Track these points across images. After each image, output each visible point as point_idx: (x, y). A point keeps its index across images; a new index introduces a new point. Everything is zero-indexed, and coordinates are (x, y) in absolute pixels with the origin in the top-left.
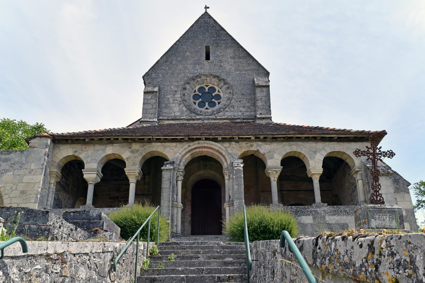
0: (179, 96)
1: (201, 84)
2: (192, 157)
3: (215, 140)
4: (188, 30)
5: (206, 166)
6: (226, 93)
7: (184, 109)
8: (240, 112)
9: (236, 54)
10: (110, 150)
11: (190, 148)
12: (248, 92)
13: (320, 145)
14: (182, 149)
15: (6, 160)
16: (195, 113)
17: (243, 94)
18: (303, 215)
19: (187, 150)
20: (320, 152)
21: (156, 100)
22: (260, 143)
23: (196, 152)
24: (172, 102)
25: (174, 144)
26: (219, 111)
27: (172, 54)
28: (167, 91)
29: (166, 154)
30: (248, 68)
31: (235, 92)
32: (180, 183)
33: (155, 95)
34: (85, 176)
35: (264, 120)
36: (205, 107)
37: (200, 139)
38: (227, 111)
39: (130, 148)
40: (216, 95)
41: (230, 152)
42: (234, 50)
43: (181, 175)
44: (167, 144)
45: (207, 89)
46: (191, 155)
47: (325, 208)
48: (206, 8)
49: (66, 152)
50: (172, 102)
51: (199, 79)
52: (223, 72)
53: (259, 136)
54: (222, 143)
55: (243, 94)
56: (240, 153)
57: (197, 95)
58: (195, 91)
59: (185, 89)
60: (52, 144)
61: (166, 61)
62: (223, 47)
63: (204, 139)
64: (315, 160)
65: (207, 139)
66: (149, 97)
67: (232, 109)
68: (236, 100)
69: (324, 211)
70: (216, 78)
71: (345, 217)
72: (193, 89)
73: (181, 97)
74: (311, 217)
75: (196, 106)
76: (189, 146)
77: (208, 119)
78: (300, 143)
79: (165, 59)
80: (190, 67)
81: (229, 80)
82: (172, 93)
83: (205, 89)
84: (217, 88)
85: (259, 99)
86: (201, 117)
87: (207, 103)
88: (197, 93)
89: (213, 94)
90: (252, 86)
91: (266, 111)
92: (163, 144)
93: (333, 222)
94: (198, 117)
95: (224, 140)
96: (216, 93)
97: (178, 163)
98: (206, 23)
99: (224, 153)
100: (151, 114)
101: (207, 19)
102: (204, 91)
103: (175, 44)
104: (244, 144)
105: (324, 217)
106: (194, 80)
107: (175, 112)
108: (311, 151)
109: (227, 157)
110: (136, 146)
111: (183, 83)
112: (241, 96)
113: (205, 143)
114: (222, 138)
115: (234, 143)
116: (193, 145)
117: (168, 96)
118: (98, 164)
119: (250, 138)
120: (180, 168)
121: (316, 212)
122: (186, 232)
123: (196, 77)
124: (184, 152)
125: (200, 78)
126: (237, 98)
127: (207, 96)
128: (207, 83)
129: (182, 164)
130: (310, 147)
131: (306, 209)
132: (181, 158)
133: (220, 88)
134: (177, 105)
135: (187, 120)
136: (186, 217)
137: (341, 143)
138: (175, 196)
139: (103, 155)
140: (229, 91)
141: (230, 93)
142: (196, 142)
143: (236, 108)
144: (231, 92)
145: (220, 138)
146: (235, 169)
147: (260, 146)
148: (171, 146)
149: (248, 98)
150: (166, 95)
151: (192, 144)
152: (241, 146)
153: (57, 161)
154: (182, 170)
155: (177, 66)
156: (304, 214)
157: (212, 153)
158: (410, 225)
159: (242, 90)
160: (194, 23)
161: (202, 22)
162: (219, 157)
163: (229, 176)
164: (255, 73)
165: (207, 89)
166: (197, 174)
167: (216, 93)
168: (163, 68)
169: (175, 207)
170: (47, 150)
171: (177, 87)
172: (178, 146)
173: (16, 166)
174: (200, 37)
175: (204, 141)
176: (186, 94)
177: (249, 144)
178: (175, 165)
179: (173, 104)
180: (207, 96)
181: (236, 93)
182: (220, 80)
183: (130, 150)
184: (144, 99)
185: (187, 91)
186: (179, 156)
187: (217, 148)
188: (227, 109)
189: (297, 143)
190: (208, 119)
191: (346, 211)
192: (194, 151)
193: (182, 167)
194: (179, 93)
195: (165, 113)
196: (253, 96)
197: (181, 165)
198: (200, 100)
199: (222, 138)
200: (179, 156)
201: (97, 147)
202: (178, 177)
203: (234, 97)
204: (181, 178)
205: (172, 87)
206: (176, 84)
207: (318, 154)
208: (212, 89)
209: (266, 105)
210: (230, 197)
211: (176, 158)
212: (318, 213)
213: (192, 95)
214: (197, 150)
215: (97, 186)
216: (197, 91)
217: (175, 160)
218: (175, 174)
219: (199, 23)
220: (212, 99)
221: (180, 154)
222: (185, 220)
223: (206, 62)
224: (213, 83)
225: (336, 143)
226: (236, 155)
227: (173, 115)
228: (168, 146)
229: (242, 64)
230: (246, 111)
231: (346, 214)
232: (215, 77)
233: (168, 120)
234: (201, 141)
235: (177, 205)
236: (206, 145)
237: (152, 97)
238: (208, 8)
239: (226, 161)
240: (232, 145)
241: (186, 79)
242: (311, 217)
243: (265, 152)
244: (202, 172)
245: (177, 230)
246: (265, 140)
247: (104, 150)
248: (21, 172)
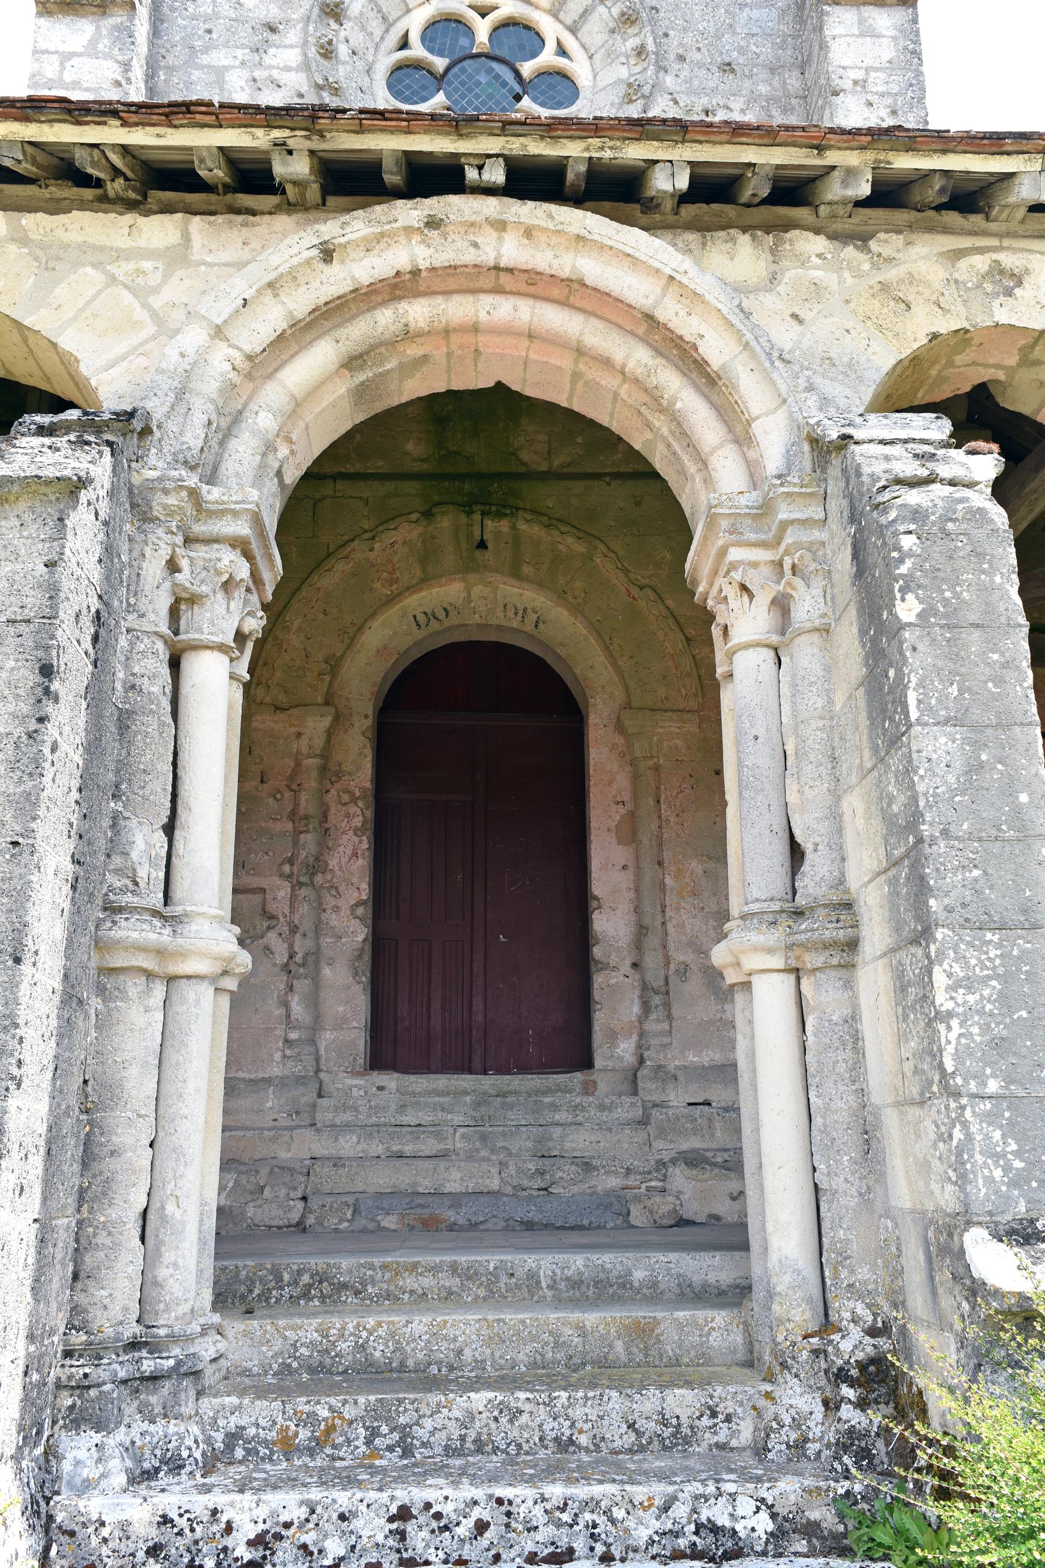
0: (292, 57)
2: (360, 393)
5: (482, 545)
6: (611, 56)
12: (766, 50)
14: (242, 286)
17: (728, 67)
19: (301, 301)
21: (127, 66)
23: (408, 335)
25: (158, 230)
28: (207, 18)
29: (67, 342)
31: (673, 45)
32: (215, 688)
33: (118, 28)
40: (543, 74)
41: (785, 335)
43: (228, 586)
44: (85, 227)
45: (482, 29)
46: (352, 362)
54: (692, 237)
55: (728, 67)
56: (883, 358)
57: (416, 65)
58: (404, 44)
63: (496, 175)
65: (533, 181)
72: (388, 24)
73: (306, 66)
76: (327, 254)
82: (244, 34)
83: (469, 31)
84: (550, 29)
85: (847, 84)
88: (417, 51)
89: (527, 69)
90: (783, 12)
92: (29, 221)
96: (548, 57)
97: (194, 437)
99: (716, 349)
102: (464, 42)
109: (752, 391)
112: (715, 79)
113: (500, 226)
115: (812, 244)
116: (369, 245)
117: (219, 58)
120: (212, 494)
122: (328, 1035)
124: (269, 320)
126: (690, 92)
127: (483, 78)
129: (242, 455)
132: (230, 389)
133: (573, 30)
136: (332, 918)
138: (144, 842)
140: (633, 42)
141: (640, 52)
142: (409, 212)
144: (651, 47)
145: (668, 182)
146: (917, 514)
148: (121, 255)
149: (763, 89)
150: (206, 50)
151: (356, 225)
152: (891, 274)
154: (242, 528)
157: (580, 351)
159: (718, 37)
162: (654, 398)
163: (782, 605)
165: (482, 29)
166: (417, 602)
167: (548, 57)
169: (134, 986)
172: (197, 252)
175: (492, 205)
176: (343, 50)
177: (981, 262)
178: (154, 466)
180: (483, 78)
181: (681, 58)
186: (202, 359)
187: (636, 289)
192: (385, 319)
193: (250, 489)
194: (293, 36)
196: (794, 82)
197: (229, 467)
200: (202, 359)
202: (194, 600)
203: (669, 81)
204: (228, 617)
210: (796, 853)
211: (166, 384)
214: (418, 312)
216: (414, 38)
217: (157, 408)
218: (153, 568)
220: (518, 98)
221: (219, 332)
222: (326, 941)
226: (851, 369)
228: (84, 247)
235: (161, 953)
236: (511, 251)
237: (93, 42)
239: (740, 432)
240: (803, 262)
244: (450, 591)
245: (148, 1288)
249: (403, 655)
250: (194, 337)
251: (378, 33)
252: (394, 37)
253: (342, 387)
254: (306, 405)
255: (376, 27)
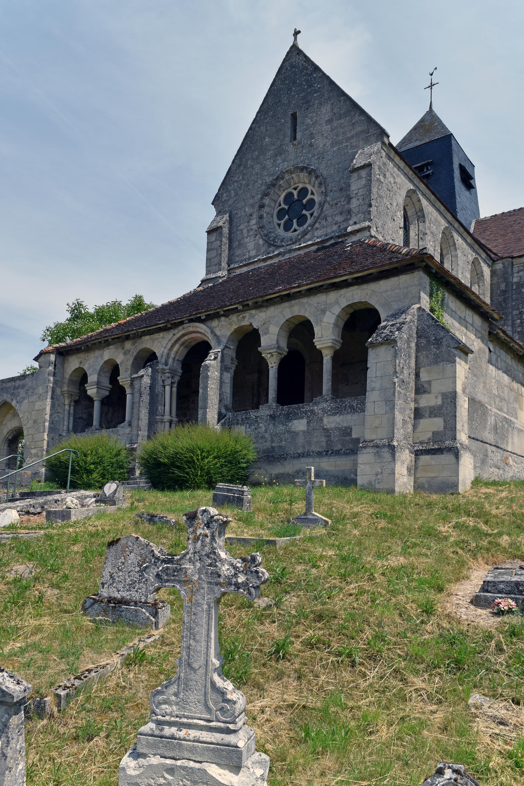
1: (287, 189)
3: (199, 320)
4: (267, 95)
7: (261, 242)
8: (336, 224)
9: (335, 111)
10: (107, 354)
11: (175, 338)
13: (333, 296)
15: (23, 386)
16: (274, 246)
18: (296, 419)
19: (173, 341)
20: (331, 310)
22: (253, 312)
24: (246, 235)
25: (161, 334)
26: (305, 233)
27: (247, 150)
28: (240, 217)
30: (353, 132)
31: (329, 188)
34: (89, 392)
35: (358, 235)
36: (309, 216)
37: (182, 323)
38: (317, 229)
39: (123, 349)
41: (218, 333)
42: (332, 104)
44: (156, 336)
47: (324, 405)
48: (297, 33)
49: (73, 363)
50: (246, 235)
51: (281, 182)
52: (314, 156)
53: (246, 303)
59: (262, 206)
60: (60, 359)
61: (240, 166)
62: (315, 106)
64: (323, 324)
65: (191, 321)
66: (213, 239)
67: (324, 223)
68: (331, 203)
69: (323, 409)
70: (305, 171)
71: (349, 417)
72: (275, 202)
74: (304, 421)
75: (281, 231)
76: (174, 335)
77: (290, 251)
78: (305, 300)
79: (237, 161)
80: (269, 163)
81: (323, 170)
85: (354, 195)
86: (282, 250)
87: (295, 221)
91: (363, 216)
93: (333, 426)
94: (276, 253)
95: (210, 318)
97: (163, 361)
98: (293, 66)
100: (216, 265)
101: (295, 59)
103: (251, 129)
104: (234, 317)
105: (322, 420)
106: (274, 185)
107: (249, 252)
108: (318, 310)
110: (128, 345)
111: (259, 196)
114: (206, 315)
116: (178, 332)
117: (242, 227)
118: (99, 375)
119: (237, 308)
121: (312, 412)
123: (277, 179)
125: (283, 178)
126: (333, 200)
128: (295, 184)
130: (318, 303)
131: (300, 408)
134: (252, 238)
135: (264, 260)
137: (365, 286)
139: (102, 363)
142: (181, 328)
143: (329, 219)
147: (252, 316)
151: (173, 332)
153: (67, 376)
155: (253, 169)
156: (297, 416)
158: (445, 422)
160: (276, 76)
161: (287, 69)
164: (363, 139)
168: (236, 179)
170: (51, 368)
171: (252, 206)
173: (30, 393)
174: (285, 100)
175: (188, 325)
179: (247, 238)
182: (310, 173)
183: (123, 351)
184: (208, 243)
185: (267, 209)
188: (317, 225)
189: (301, 300)
190: (290, 251)
191: (351, 407)
192: (183, 340)
195: (238, 256)
198: (287, 217)
199: (206, 315)
200: (163, 352)
201: (97, 353)
205: (247, 209)
206: (251, 201)
207: (328, 313)
208: (304, 192)
209: (364, 203)
212: (314, 414)
213: (276, 211)
215: (104, 402)
219: (284, 71)
221: (165, 348)
223: (291, 148)
224: (302, 180)
225: (357, 287)
227: (247, 256)
229: (344, 127)
230: (344, 221)
231: (351, 411)
232: (302, 169)
233: (240, 267)
234: (185, 326)
236: (191, 329)
238: (299, 32)
241: (263, 187)
242: (304, 421)
243: (259, 325)
246: (258, 306)
247: (102, 356)
248: (32, 399)
249: (336, 325)
250: (163, 349)
251: (273, 205)
252: (277, 204)
253: (182, 348)
254: (179, 352)
255: (273, 204)
